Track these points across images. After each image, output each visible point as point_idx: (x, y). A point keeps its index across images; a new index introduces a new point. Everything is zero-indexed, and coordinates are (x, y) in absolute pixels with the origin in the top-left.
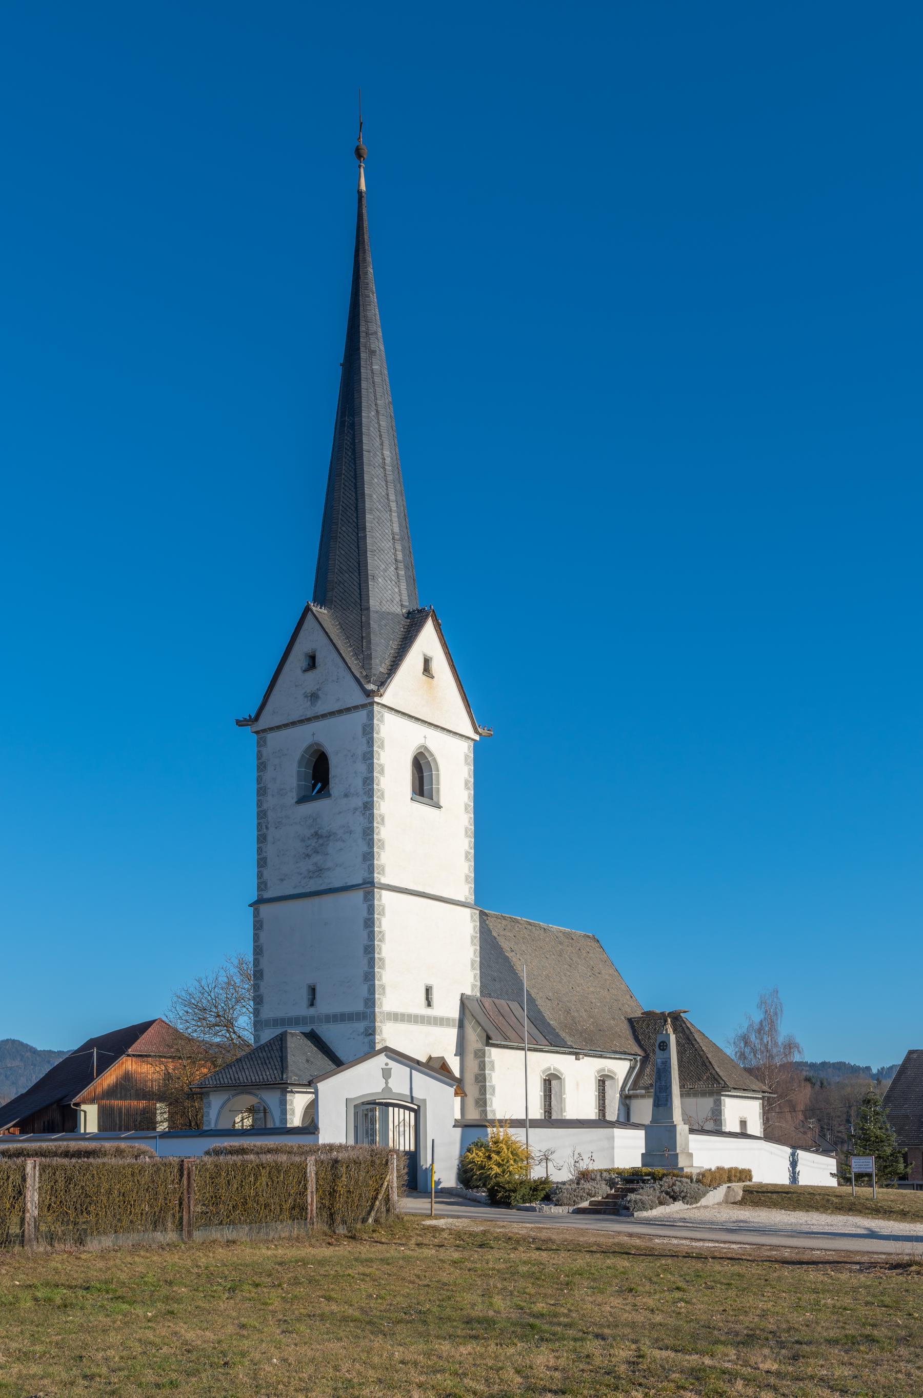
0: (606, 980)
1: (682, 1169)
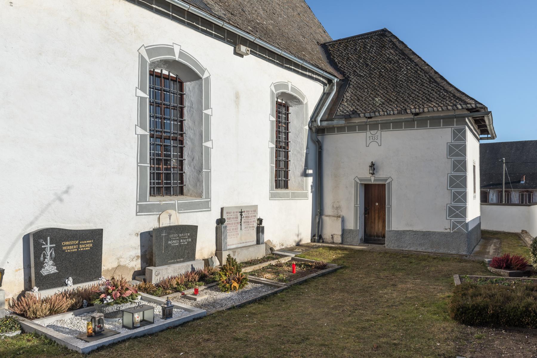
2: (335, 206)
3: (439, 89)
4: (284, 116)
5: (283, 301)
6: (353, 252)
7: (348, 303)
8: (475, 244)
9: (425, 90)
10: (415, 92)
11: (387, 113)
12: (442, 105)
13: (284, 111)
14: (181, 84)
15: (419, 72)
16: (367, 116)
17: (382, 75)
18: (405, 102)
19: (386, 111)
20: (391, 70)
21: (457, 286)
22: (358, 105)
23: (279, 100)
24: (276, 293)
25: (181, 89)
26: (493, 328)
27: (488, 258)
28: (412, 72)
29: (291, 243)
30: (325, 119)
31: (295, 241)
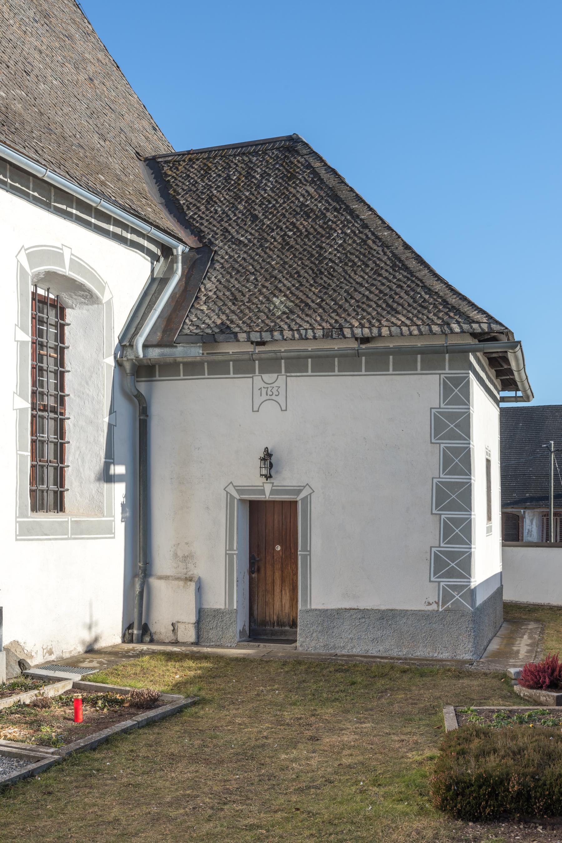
2: (180, 554)
3: (413, 285)
4: (52, 330)
5: (50, 793)
6: (222, 664)
7: (206, 790)
8: (490, 636)
9: (383, 284)
10: (362, 290)
11: (300, 335)
12: (419, 323)
13: (52, 319)
15: (370, 242)
16: (253, 339)
17: (288, 244)
18: (340, 311)
19: (298, 330)
20: (309, 233)
21: (449, 732)
22: (233, 312)
23: (41, 291)
24: (31, 774)
26: (519, 822)
27: (514, 666)
28: (354, 241)
29: (73, 647)
30: (155, 343)
31: (83, 642)
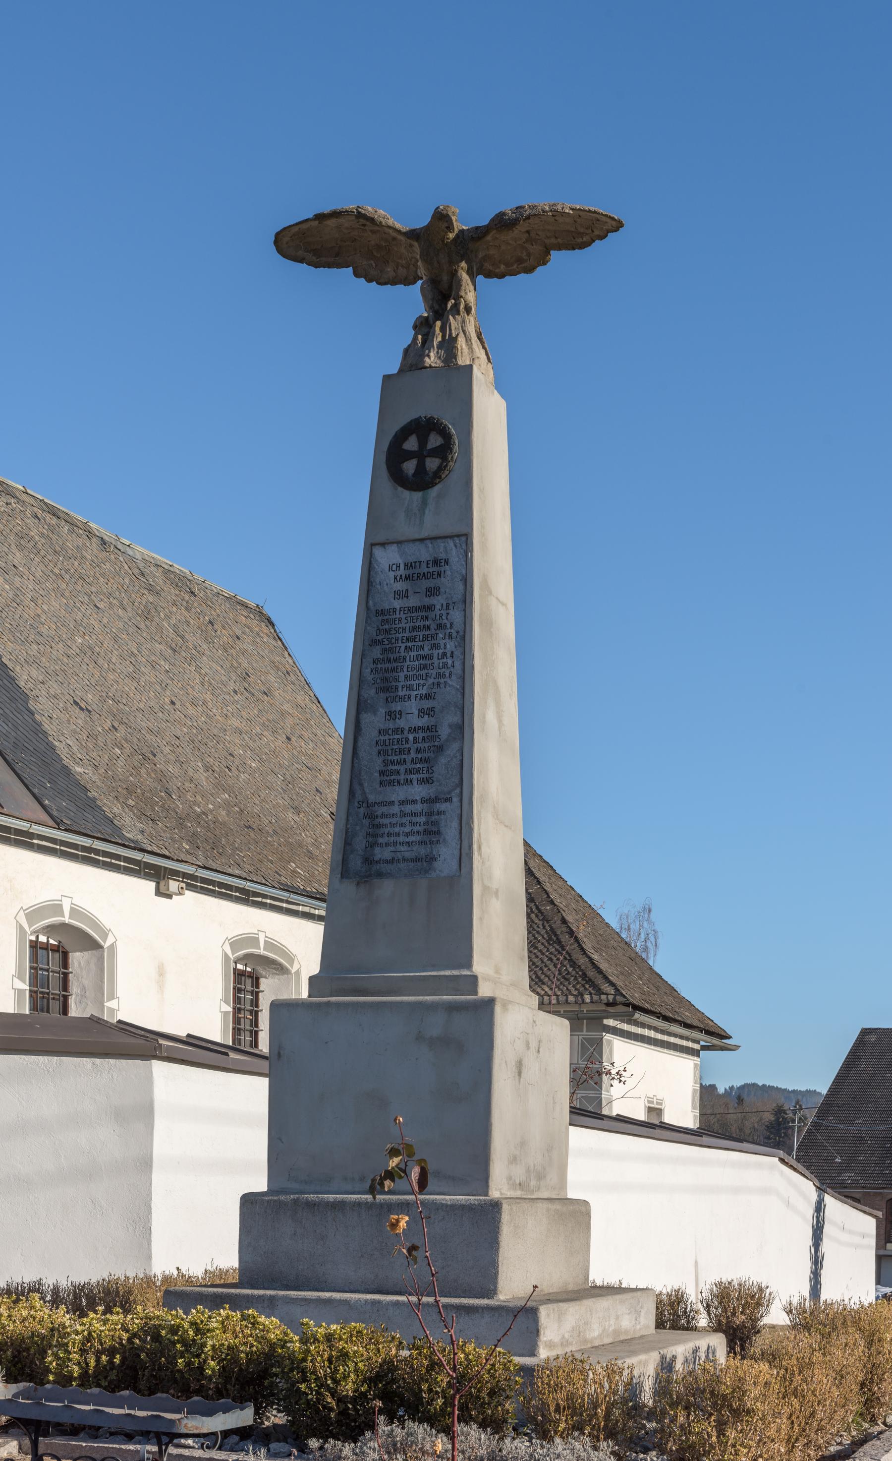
0: (283, 714)
1: (524, 1318)
4: (249, 997)
9: (537, 957)
12: (559, 993)
14: (65, 955)
23: (240, 967)
25: (65, 964)
